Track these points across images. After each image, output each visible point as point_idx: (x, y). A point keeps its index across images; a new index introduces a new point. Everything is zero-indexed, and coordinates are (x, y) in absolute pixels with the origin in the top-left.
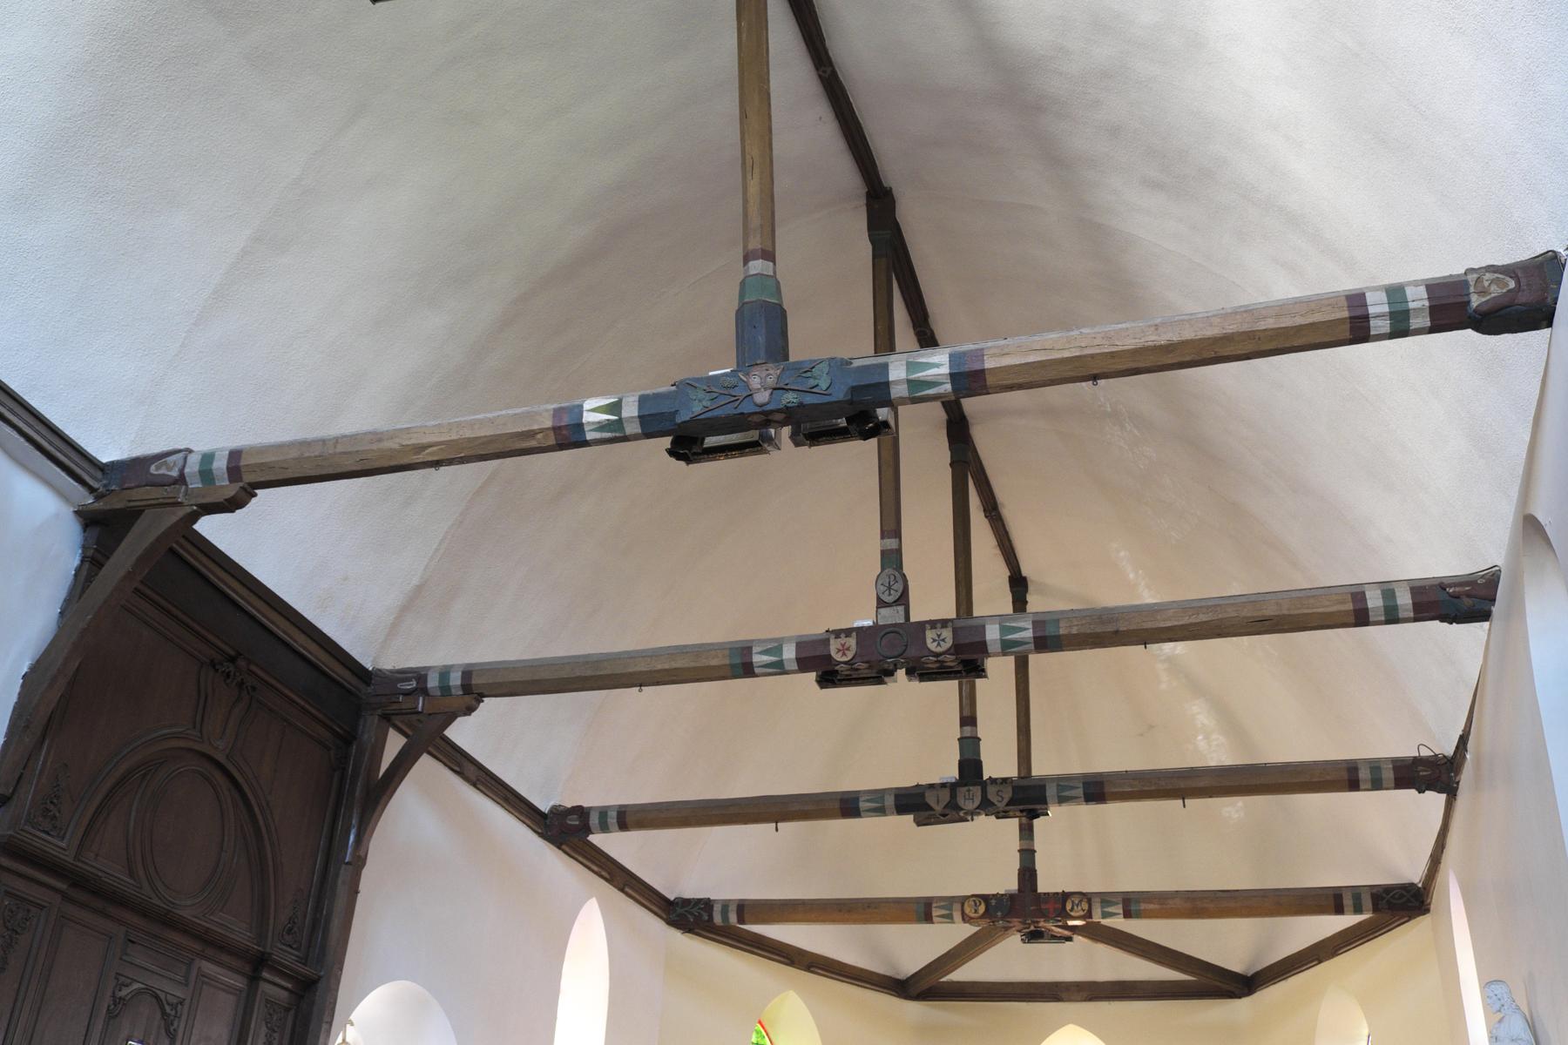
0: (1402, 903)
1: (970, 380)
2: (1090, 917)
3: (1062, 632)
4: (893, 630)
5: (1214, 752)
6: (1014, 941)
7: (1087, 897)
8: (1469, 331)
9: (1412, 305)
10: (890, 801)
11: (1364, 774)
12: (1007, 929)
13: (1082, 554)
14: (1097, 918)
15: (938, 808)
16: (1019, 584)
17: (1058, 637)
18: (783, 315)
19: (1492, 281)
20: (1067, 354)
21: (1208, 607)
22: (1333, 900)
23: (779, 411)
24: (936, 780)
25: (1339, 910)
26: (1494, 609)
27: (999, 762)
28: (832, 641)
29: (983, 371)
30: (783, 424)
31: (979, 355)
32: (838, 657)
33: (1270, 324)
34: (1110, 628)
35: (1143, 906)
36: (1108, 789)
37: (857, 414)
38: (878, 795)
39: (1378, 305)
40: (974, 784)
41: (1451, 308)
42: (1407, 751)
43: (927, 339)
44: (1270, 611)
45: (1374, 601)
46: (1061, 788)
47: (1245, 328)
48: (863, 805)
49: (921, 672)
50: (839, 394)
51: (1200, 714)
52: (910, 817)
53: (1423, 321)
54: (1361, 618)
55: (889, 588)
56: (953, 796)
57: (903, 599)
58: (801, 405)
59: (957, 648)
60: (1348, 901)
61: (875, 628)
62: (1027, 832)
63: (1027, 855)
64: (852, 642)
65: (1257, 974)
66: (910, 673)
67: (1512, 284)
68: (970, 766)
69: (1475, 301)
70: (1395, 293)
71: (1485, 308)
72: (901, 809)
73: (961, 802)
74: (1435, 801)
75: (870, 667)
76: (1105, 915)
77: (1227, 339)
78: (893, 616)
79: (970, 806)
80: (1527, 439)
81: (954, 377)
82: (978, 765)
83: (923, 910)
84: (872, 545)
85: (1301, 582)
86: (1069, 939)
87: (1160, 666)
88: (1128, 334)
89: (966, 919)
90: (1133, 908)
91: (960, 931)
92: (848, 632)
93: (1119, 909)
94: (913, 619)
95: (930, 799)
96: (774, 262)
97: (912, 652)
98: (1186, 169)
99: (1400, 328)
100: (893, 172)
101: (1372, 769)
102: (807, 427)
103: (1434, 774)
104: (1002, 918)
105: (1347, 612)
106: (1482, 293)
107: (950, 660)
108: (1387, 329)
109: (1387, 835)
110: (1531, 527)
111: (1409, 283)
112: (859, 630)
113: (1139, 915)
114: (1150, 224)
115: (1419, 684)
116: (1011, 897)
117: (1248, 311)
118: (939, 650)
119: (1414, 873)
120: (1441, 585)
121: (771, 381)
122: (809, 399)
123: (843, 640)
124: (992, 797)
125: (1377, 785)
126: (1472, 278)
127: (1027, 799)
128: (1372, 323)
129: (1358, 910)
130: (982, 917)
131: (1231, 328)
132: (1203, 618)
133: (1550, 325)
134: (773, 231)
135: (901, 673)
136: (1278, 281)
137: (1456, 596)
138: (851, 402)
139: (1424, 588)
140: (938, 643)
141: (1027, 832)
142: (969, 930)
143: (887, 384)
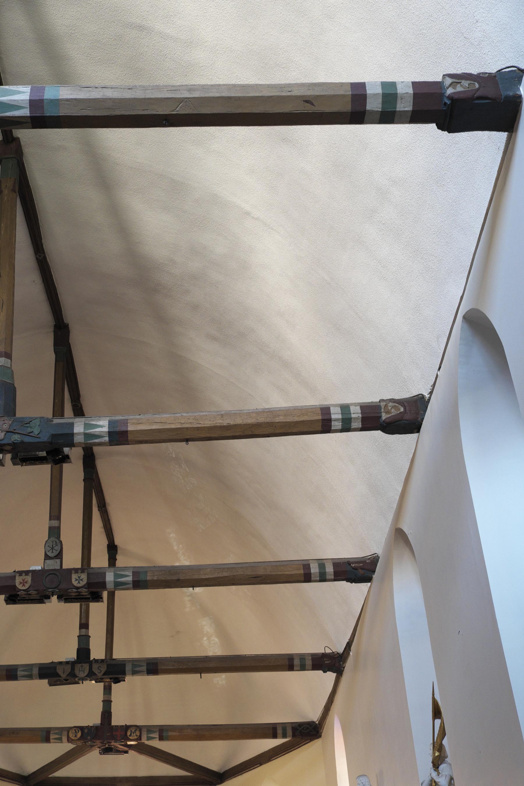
0: (307, 732)
1: (119, 437)
2: (141, 739)
3: (149, 578)
4: (52, 573)
5: (212, 647)
6: (95, 753)
7: (139, 728)
8: (379, 431)
9: (353, 416)
10: (36, 671)
11: (297, 662)
12: (92, 746)
13: (150, 536)
14: (144, 740)
15: (64, 676)
16: (112, 549)
17: (146, 581)
18: (15, 389)
19: (393, 407)
20: (173, 426)
21: (228, 568)
22: (272, 730)
23: (9, 444)
24: (63, 660)
25: (275, 736)
26: (374, 576)
27: (97, 652)
28: (17, 578)
29: (127, 432)
30: (9, 452)
31: (125, 422)
32: (20, 587)
33: (281, 419)
34: (175, 578)
35: (170, 733)
36: (161, 667)
37: (52, 451)
38: (29, 667)
39: (336, 414)
40: (85, 663)
41: (373, 419)
42: (319, 650)
43: (79, 412)
44: (261, 572)
45: (314, 569)
46: (134, 666)
47: (268, 420)
48: (19, 673)
49: (66, 597)
50: (45, 438)
51: (207, 626)
52: (46, 681)
53: (357, 424)
54: (307, 578)
55: (52, 549)
56: (73, 669)
57: (59, 556)
58: (22, 442)
59: (89, 585)
60: (280, 731)
61: (43, 571)
62: (108, 690)
63: (107, 703)
64: (29, 578)
65: (226, 772)
66: (60, 598)
67: (402, 409)
68: (83, 652)
69: (384, 416)
70: (345, 408)
71: (388, 421)
72: (41, 676)
73: (77, 672)
74: (331, 676)
75: (38, 594)
76: (149, 739)
77: (258, 425)
78: (53, 565)
79: (82, 675)
80: (400, 489)
81: (110, 433)
82: (88, 651)
83: (45, 735)
84: (44, 523)
85: (269, 558)
86: (126, 752)
87: (187, 599)
88: (205, 418)
89: (69, 740)
90: (164, 734)
91: (66, 747)
92: (27, 573)
93: (156, 735)
94: (64, 567)
95: (60, 671)
96: (11, 359)
97: (63, 586)
98: (231, 332)
99: (346, 427)
100: (70, 315)
101: (301, 659)
102: (21, 455)
103: (331, 663)
104: (90, 741)
105: (300, 574)
106: (388, 412)
107: (84, 592)
108: (340, 427)
109: (303, 694)
110: (399, 535)
111: (352, 404)
112: (34, 572)
113: (168, 739)
114: (208, 358)
115: (327, 614)
116: (96, 728)
117: (270, 411)
118: (79, 585)
119: (314, 716)
120: (348, 562)
121: (6, 427)
122: (27, 439)
123: (24, 577)
124: (95, 670)
125: (303, 668)
126: (383, 404)
127: (114, 671)
128: (333, 423)
129: (284, 736)
130: (79, 739)
131: (261, 420)
132: (225, 574)
133: (418, 431)
134: (12, 342)
135: (54, 598)
136: (275, 397)
137: (355, 569)
138: (51, 443)
139: (339, 563)
140: (79, 581)
141: (108, 690)
142: (70, 746)
143: (72, 435)
